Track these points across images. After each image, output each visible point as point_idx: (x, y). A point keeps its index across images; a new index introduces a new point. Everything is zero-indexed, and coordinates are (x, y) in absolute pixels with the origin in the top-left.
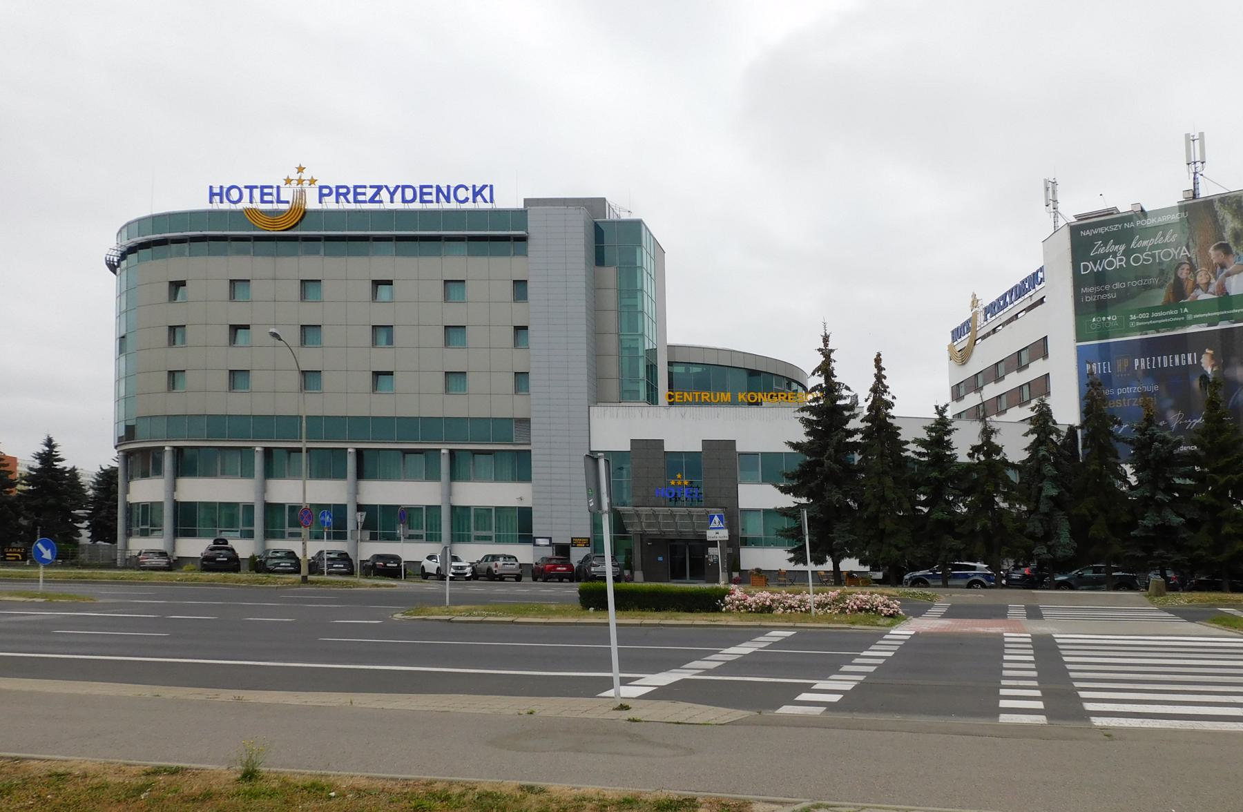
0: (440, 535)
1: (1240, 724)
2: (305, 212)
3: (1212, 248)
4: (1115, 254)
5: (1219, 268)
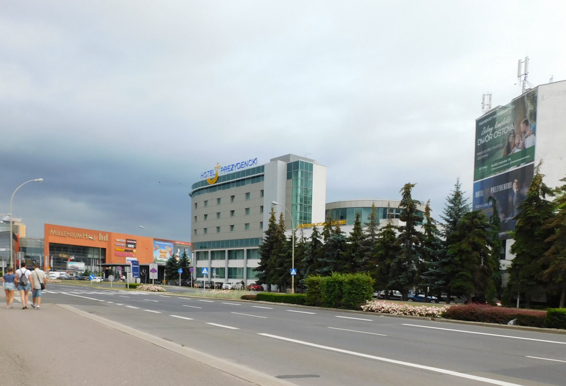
0: (224, 276)
1: (1, 288)
2: (218, 177)
3: (522, 123)
4: (489, 133)
5: (523, 133)
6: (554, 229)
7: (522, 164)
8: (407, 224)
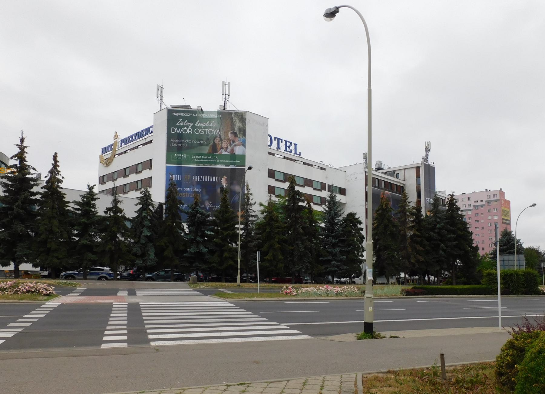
6: (153, 243)
7: (231, 165)
8: (299, 203)
